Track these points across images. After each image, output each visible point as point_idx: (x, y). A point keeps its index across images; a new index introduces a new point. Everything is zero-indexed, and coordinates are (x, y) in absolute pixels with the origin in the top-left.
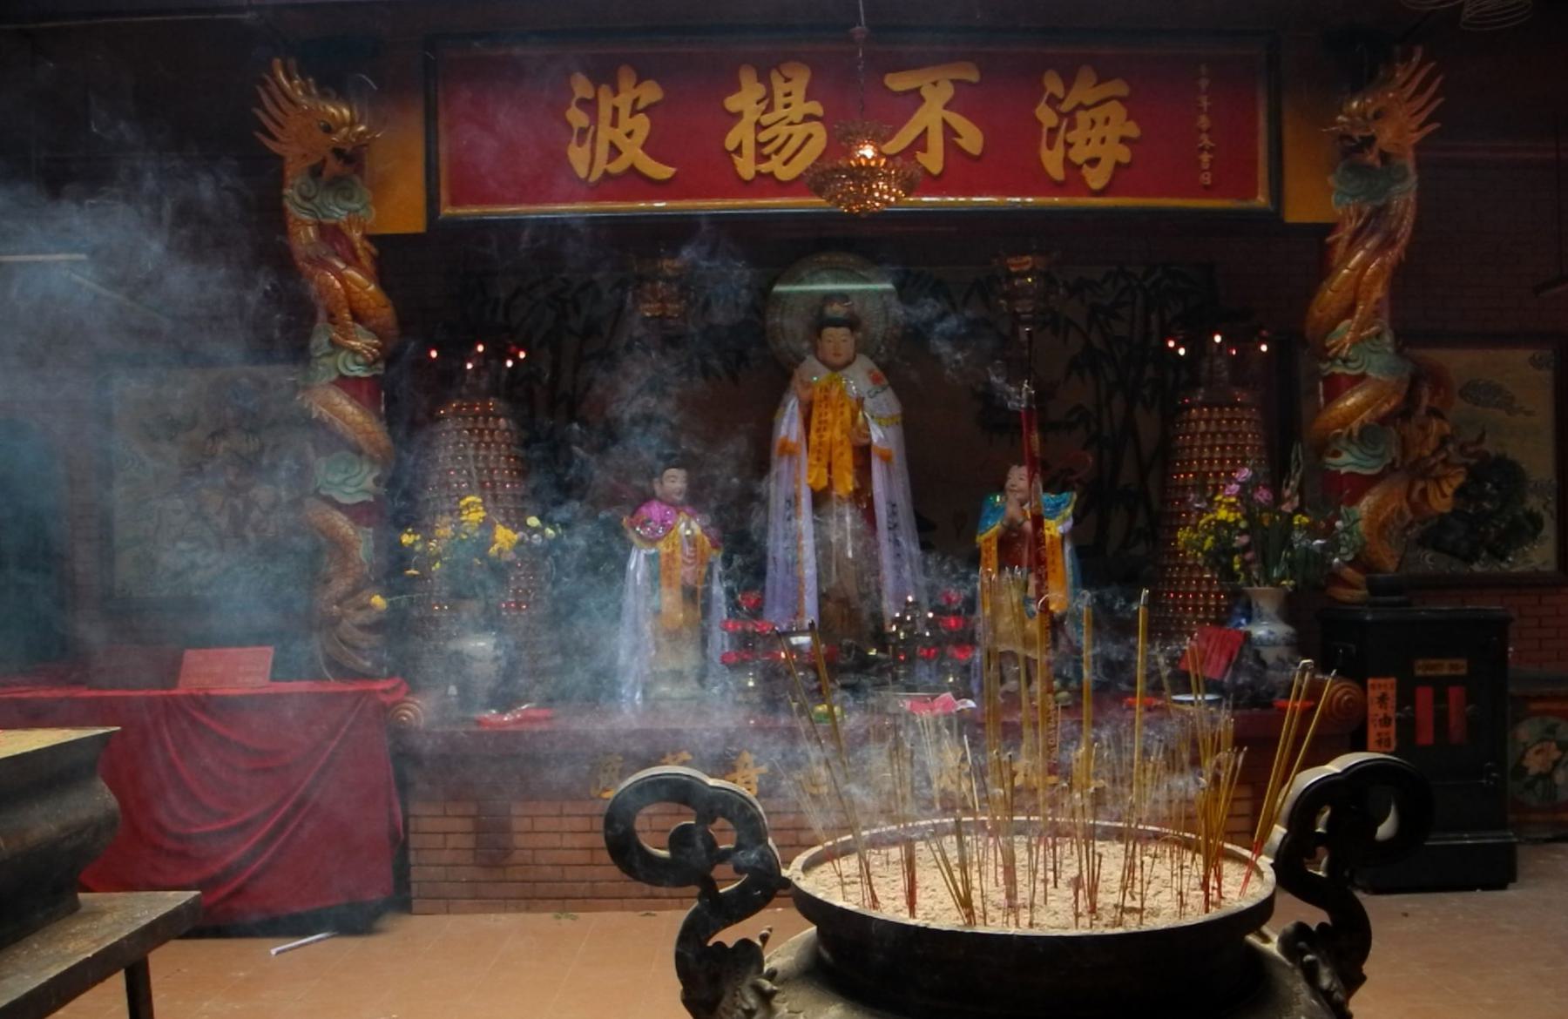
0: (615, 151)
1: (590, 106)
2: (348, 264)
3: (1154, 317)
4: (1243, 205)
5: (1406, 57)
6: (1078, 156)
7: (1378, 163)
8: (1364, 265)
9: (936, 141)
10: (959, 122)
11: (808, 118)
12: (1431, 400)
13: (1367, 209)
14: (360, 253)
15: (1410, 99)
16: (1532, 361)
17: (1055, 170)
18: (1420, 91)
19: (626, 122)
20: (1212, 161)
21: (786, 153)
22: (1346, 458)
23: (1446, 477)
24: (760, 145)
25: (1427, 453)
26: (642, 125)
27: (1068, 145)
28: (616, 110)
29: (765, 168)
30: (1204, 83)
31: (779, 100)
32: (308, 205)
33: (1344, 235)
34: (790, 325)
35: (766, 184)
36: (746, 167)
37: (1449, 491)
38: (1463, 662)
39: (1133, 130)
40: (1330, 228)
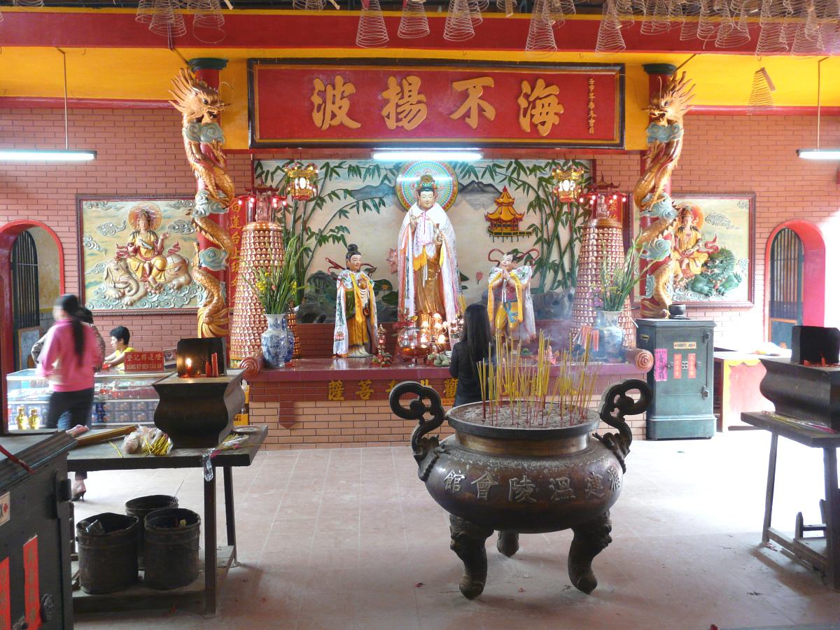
0: (334, 116)
6: (536, 120)
7: (666, 125)
9: (474, 113)
10: (484, 104)
11: (419, 102)
19: (339, 102)
24: (398, 114)
25: (690, 247)
26: (346, 104)
27: (532, 116)
28: (334, 95)
29: (400, 124)
31: (406, 94)
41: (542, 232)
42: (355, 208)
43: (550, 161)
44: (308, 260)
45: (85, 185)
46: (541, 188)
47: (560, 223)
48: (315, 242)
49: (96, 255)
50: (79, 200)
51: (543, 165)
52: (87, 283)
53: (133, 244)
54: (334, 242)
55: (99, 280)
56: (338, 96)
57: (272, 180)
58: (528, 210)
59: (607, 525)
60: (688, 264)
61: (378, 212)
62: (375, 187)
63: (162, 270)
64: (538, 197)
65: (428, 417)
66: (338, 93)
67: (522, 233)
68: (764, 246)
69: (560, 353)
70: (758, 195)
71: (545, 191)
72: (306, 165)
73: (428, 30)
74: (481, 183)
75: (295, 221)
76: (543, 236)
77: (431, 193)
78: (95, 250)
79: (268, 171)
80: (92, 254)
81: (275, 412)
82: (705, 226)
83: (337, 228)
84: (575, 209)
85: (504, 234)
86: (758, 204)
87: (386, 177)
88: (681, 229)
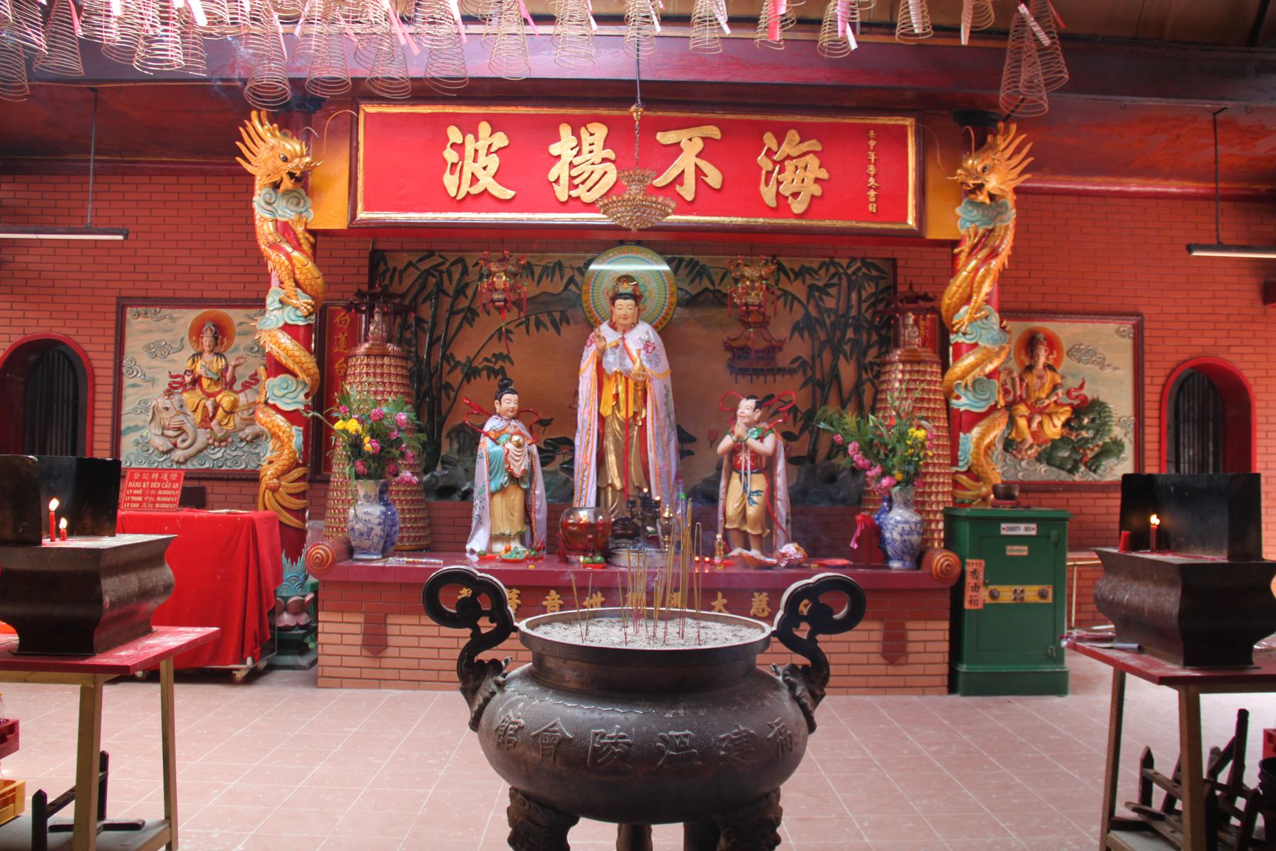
0: (474, 180)
1: (459, 148)
2: (294, 249)
3: (854, 295)
4: (897, 227)
5: (1007, 130)
6: (786, 190)
7: (988, 201)
8: (976, 269)
9: (690, 179)
10: (706, 166)
11: (605, 160)
12: (1047, 358)
13: (981, 231)
14: (302, 241)
15: (1009, 159)
16: (1118, 331)
17: (770, 199)
18: (1017, 151)
19: (482, 159)
20: (876, 196)
21: (589, 184)
22: (963, 400)
23: (1056, 413)
24: (572, 178)
25: (1043, 395)
26: (494, 162)
27: (779, 183)
28: (476, 151)
29: (574, 193)
30: (872, 143)
31: (586, 148)
32: (269, 208)
33: (965, 248)
34: (597, 297)
35: (574, 204)
36: (562, 193)
37: (1059, 423)
38: (1026, 548)
39: (823, 174)
40: (955, 243)
41: (813, 368)
42: (523, 327)
43: (827, 260)
44: (449, 403)
45: (434, 653)
46: (812, 301)
47: (842, 357)
48: (461, 376)
49: (139, 386)
50: (122, 306)
51: (815, 266)
52: (123, 427)
53: (192, 371)
54: (489, 377)
55: (141, 424)
56: (482, 152)
57: (401, 282)
58: (792, 334)
59: (771, 816)
60: (1041, 423)
61: (559, 333)
62: (554, 295)
63: (230, 413)
64: (807, 314)
65: (486, 626)
66: (482, 145)
67: (781, 371)
68: (1157, 397)
69: (744, 510)
70: (1146, 317)
71: (818, 307)
72: (451, 260)
73: (1067, 76)
74: (719, 291)
75: (431, 344)
76: (814, 374)
77: (631, 302)
78: (137, 381)
79: (395, 269)
80: (134, 386)
81: (358, 629)
82: (1066, 364)
83: (494, 355)
84: (865, 335)
85: (754, 370)
86: (1146, 333)
87: (571, 280)
88: (1029, 369)
